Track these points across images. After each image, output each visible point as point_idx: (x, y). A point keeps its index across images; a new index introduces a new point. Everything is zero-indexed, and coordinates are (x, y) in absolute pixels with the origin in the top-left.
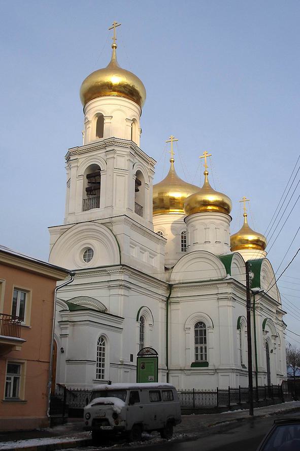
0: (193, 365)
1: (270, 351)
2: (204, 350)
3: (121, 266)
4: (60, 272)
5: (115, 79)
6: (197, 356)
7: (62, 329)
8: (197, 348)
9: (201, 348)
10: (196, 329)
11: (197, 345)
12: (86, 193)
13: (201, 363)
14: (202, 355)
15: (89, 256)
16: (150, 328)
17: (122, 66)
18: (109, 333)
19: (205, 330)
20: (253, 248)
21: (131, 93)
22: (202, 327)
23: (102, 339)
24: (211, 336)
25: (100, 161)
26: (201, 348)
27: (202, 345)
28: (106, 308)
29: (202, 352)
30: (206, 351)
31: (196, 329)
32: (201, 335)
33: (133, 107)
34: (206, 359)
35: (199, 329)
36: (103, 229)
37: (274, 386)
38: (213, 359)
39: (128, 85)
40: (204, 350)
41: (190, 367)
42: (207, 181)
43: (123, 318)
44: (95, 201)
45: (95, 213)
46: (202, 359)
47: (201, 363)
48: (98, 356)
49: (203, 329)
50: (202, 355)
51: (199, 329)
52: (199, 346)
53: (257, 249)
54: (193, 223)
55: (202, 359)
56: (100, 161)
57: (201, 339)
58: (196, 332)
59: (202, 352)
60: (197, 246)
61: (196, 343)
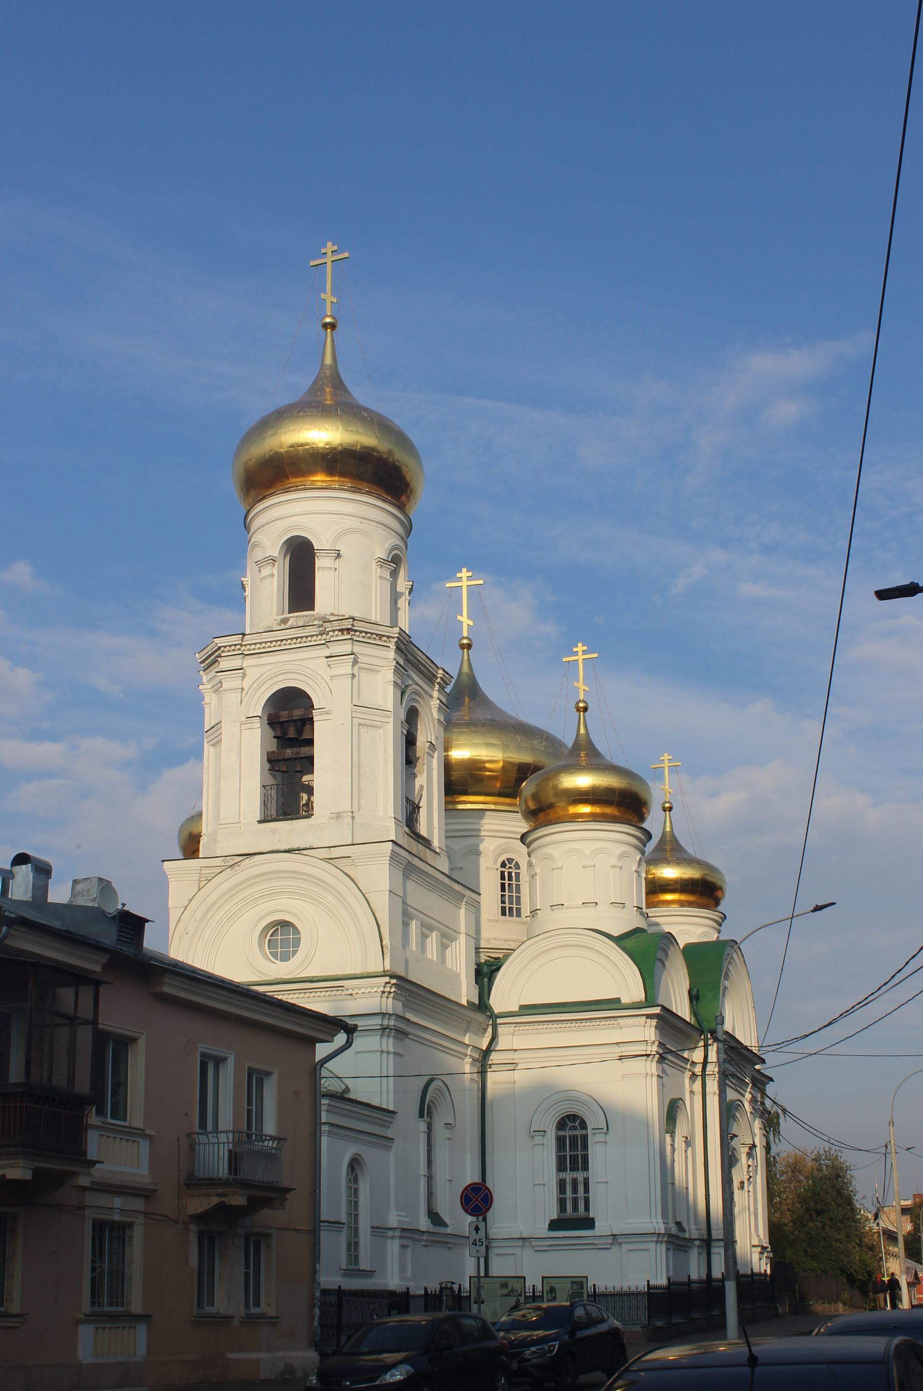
0: (554, 1225)
1: (736, 1184)
2: (581, 1188)
3: (387, 979)
4: (328, 1025)
5: (321, 434)
6: (562, 1203)
7: (216, 1130)
8: (562, 1185)
9: (575, 1182)
10: (560, 1133)
11: (562, 1175)
12: (267, 766)
13: (573, 1219)
14: (575, 1201)
15: (285, 943)
16: (448, 1133)
17: (361, 394)
18: (369, 1154)
19: (585, 1138)
20: (681, 904)
21: (379, 474)
22: (574, 1128)
23: (355, 1164)
24: (599, 1154)
25: (311, 682)
26: (575, 1182)
27: (575, 1175)
28: (347, 1087)
29: (575, 1190)
30: (586, 1190)
31: (560, 1133)
32: (573, 1147)
33: (348, 507)
34: (587, 1208)
35: (567, 1133)
36: (328, 873)
37: (695, 1282)
38: (608, 1212)
39: (373, 449)
40: (581, 1188)
41: (546, 1230)
42: (582, 731)
43: (393, 1112)
44: (728, 950)
45: (289, 832)
46: (575, 1208)
47: (573, 1219)
48: (380, 1229)
49: (579, 1132)
50: (575, 1201)
51: (567, 1133)
52: (568, 1176)
53: (690, 904)
54: (550, 850)
55: (575, 1208)
56: (311, 682)
57: (574, 1159)
58: (560, 1141)
59: (575, 1190)
60: (559, 914)
61: (561, 1167)
